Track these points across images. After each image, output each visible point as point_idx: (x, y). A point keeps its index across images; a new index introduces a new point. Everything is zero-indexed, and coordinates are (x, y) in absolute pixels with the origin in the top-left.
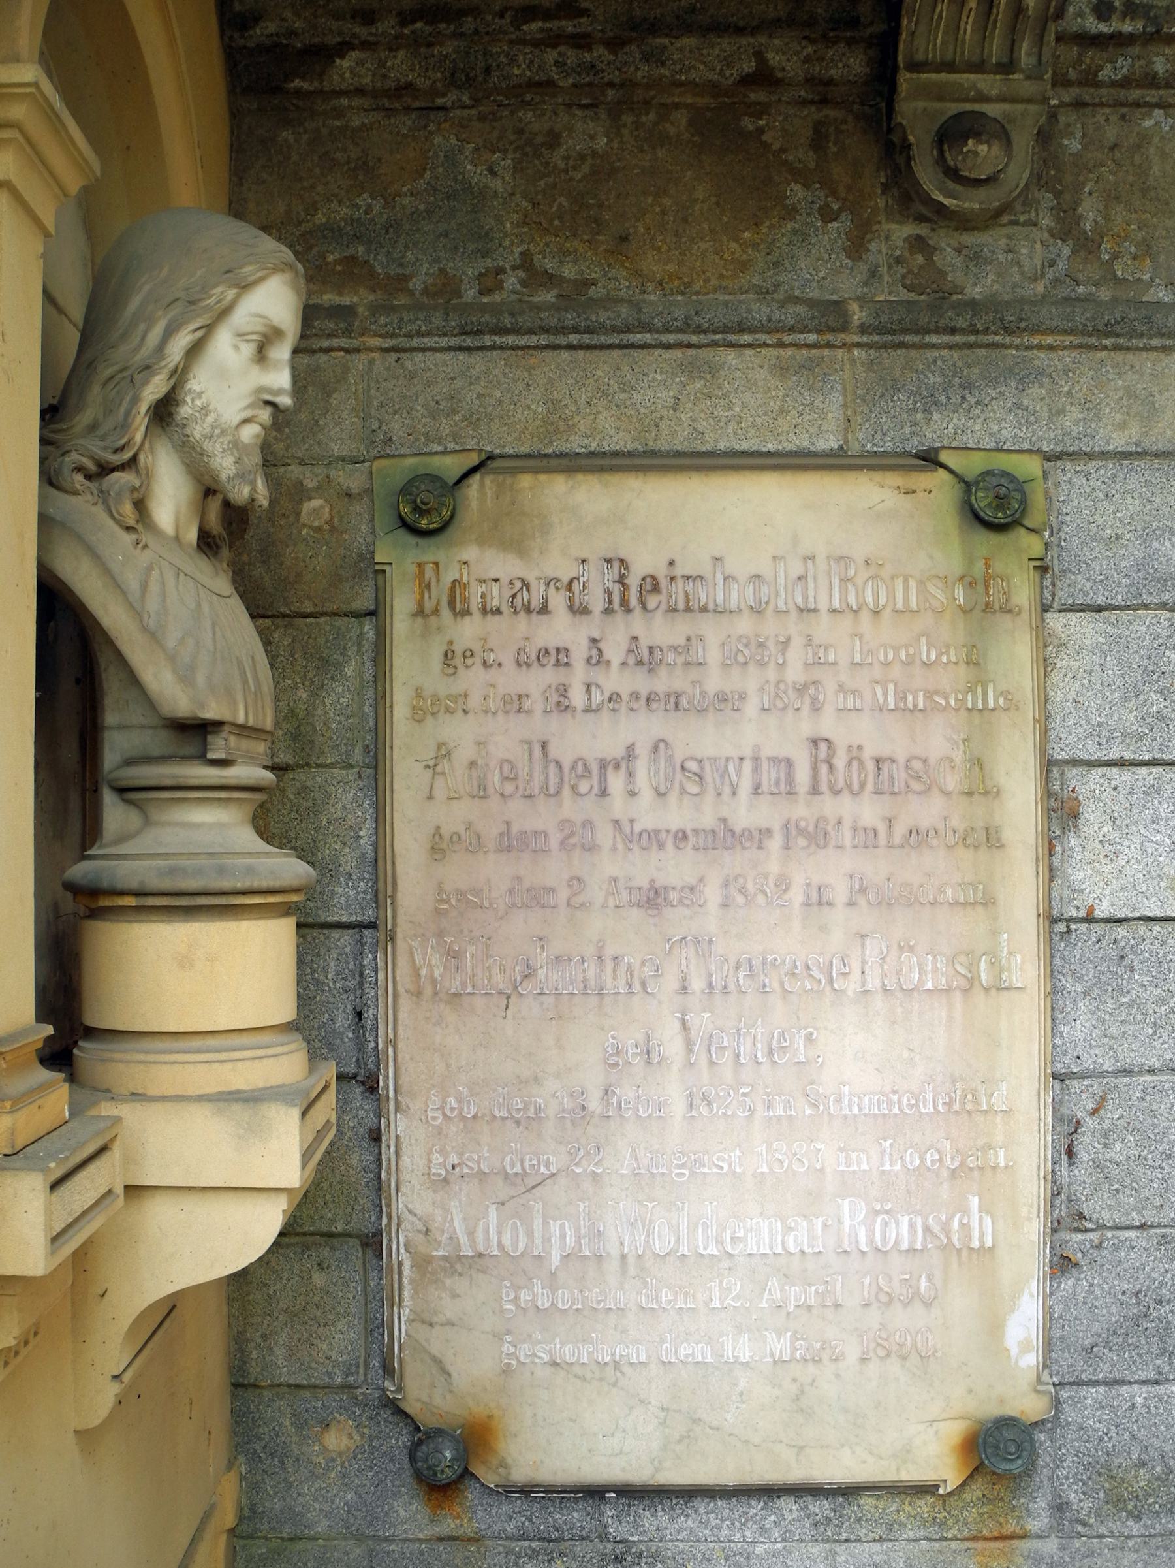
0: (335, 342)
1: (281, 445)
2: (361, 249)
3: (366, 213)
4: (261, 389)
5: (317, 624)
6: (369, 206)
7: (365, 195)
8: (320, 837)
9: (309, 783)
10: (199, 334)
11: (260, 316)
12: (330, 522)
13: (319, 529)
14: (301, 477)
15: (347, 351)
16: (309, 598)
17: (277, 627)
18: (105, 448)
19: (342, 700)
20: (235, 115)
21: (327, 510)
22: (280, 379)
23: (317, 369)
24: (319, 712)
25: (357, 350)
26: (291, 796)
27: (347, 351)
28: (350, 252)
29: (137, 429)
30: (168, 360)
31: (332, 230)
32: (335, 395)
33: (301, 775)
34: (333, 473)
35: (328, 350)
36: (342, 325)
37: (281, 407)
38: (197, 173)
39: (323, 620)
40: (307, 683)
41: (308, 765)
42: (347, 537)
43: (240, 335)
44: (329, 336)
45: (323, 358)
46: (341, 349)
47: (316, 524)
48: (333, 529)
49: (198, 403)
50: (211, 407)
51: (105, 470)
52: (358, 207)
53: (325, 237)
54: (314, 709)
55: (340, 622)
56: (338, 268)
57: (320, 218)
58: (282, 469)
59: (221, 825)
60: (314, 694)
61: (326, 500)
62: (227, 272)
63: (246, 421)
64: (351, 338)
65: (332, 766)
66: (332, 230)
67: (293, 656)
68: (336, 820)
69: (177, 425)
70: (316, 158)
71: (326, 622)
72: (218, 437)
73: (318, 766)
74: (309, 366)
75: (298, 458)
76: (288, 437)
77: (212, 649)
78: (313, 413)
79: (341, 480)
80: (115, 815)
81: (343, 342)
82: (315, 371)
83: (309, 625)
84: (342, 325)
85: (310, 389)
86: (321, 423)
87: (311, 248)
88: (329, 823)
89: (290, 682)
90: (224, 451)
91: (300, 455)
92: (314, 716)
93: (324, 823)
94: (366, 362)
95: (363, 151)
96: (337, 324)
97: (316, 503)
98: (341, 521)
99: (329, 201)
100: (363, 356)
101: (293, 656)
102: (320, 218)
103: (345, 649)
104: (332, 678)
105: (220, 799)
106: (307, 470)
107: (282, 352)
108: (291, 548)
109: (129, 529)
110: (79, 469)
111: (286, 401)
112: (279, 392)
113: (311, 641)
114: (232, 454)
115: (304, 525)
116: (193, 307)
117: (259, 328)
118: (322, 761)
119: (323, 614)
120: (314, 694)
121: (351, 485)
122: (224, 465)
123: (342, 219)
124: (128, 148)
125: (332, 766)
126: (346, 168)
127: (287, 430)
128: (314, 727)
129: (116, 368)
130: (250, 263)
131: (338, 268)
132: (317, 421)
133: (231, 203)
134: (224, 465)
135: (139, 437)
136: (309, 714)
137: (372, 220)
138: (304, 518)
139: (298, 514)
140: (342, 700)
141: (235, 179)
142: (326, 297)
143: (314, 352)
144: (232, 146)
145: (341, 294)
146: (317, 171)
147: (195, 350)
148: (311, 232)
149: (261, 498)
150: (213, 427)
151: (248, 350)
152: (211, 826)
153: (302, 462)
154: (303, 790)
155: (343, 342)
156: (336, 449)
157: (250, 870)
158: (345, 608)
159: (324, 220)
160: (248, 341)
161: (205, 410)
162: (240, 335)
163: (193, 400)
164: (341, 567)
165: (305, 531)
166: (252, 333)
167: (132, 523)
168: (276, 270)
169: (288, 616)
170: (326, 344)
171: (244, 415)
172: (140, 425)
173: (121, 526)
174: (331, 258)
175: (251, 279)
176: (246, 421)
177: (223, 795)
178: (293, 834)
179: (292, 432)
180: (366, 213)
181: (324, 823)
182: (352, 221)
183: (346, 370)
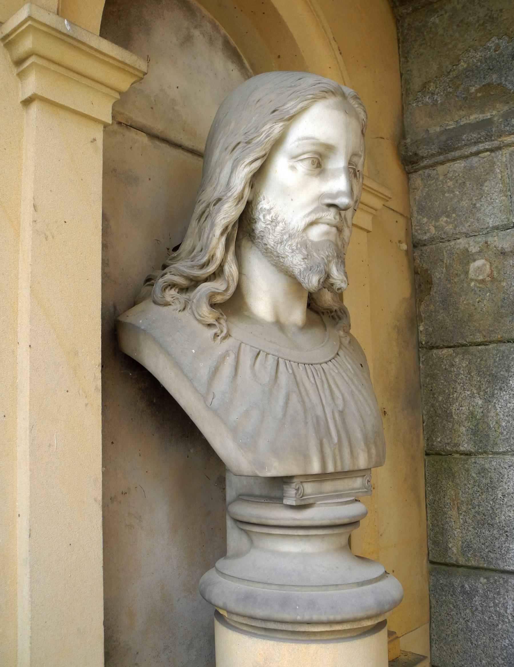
0: (481, 146)
1: (451, 226)
2: (494, 76)
3: (495, 51)
4: (321, 196)
5: (486, 349)
6: (498, 46)
7: (493, 39)
8: (497, 506)
9: (487, 466)
10: (257, 164)
11: (307, 138)
12: (491, 275)
13: (483, 281)
14: (467, 246)
15: (491, 150)
16: (480, 332)
17: (457, 354)
18: (192, 267)
19: (509, 405)
20: (398, 20)
21: (488, 266)
22: (338, 184)
23: (472, 168)
24: (492, 414)
25: (499, 148)
26: (474, 475)
27: (491, 150)
28: (487, 81)
29: (216, 248)
30: (233, 190)
31: (472, 71)
32: (486, 184)
33: (481, 460)
34: (490, 239)
35: (477, 154)
36: (483, 133)
37: (341, 206)
38: (336, 58)
39: (491, 346)
40: (482, 393)
41: (485, 452)
42: (504, 284)
43: (294, 157)
44: (476, 143)
45: (475, 160)
46: (487, 150)
47: (481, 277)
48: (493, 279)
49: (268, 217)
50: (279, 219)
51: (195, 283)
52: (489, 49)
53: (467, 77)
54: (488, 412)
55: (503, 347)
56: (479, 95)
57: (463, 65)
58: (452, 243)
59: (305, 555)
60: (487, 401)
61: (486, 260)
62: (274, 111)
63: (312, 224)
64: (492, 141)
65: (504, 453)
66: (472, 71)
67: (470, 374)
68: (509, 494)
69: (258, 237)
70: (455, 27)
71: (493, 348)
72: (287, 241)
73: (494, 453)
74: (465, 167)
75: (464, 233)
76: (455, 220)
77: (280, 415)
78: (471, 200)
79: (496, 243)
80: (234, 538)
81: (487, 145)
82: (470, 170)
83: (480, 351)
84: (483, 133)
85: (468, 183)
86: (478, 205)
87: (458, 87)
88: (504, 496)
89: (469, 393)
90: (293, 251)
91: (464, 230)
92: (488, 417)
93: (500, 495)
94: (508, 155)
95: (488, 9)
96: (479, 134)
97: (479, 263)
98: (499, 273)
99: (468, 51)
100: (504, 151)
101: (470, 374)
102: (463, 65)
103: (509, 367)
104: (501, 389)
105: (299, 536)
106: (471, 240)
107: (338, 163)
108: (463, 297)
109: (210, 325)
110: (172, 285)
111: (343, 201)
112: (338, 194)
113: (483, 362)
114: (301, 252)
115: (472, 280)
116: (249, 146)
117: (313, 148)
118: (496, 450)
119: (491, 342)
120: (487, 401)
121: (505, 246)
122: (295, 262)
123: (478, 60)
124: (279, 57)
125: (504, 453)
126: (477, 25)
127: (454, 215)
128: (488, 425)
129: (204, 205)
130: (291, 100)
131: (479, 95)
132: (475, 205)
133: (401, 75)
134: (296, 262)
135: (219, 254)
136: (485, 415)
137: (501, 53)
138: (472, 274)
139: (467, 273)
140: (509, 405)
141: (402, 59)
142: (472, 117)
143: (467, 157)
144: (399, 40)
145: (483, 112)
146: (457, 35)
147: (258, 177)
148: (457, 77)
149: (339, 282)
150: (282, 235)
151: (303, 167)
152: (296, 555)
153: (467, 235)
154: (483, 471)
155: (487, 145)
156: (491, 222)
157: (312, 604)
158: (506, 336)
159: (465, 66)
160: (302, 160)
161: (274, 222)
162: (294, 157)
163: (264, 216)
164: (502, 306)
165: (472, 284)
166: (304, 154)
167: (211, 321)
168: (316, 99)
169: (465, 345)
170: (474, 149)
171: (308, 220)
172: (218, 243)
173: (203, 324)
174: (473, 90)
175: (292, 112)
176: (312, 224)
177: (301, 532)
178: (476, 502)
179: (458, 216)
180: (495, 51)
181: (500, 495)
182: (486, 59)
183: (493, 164)
